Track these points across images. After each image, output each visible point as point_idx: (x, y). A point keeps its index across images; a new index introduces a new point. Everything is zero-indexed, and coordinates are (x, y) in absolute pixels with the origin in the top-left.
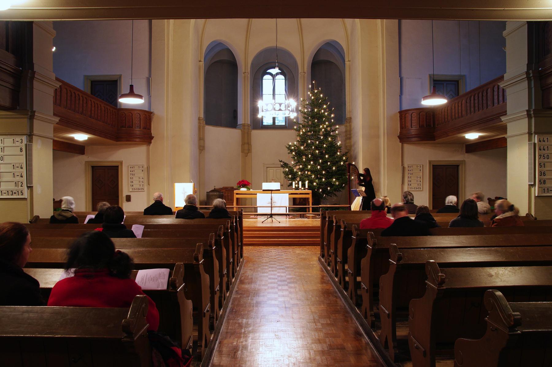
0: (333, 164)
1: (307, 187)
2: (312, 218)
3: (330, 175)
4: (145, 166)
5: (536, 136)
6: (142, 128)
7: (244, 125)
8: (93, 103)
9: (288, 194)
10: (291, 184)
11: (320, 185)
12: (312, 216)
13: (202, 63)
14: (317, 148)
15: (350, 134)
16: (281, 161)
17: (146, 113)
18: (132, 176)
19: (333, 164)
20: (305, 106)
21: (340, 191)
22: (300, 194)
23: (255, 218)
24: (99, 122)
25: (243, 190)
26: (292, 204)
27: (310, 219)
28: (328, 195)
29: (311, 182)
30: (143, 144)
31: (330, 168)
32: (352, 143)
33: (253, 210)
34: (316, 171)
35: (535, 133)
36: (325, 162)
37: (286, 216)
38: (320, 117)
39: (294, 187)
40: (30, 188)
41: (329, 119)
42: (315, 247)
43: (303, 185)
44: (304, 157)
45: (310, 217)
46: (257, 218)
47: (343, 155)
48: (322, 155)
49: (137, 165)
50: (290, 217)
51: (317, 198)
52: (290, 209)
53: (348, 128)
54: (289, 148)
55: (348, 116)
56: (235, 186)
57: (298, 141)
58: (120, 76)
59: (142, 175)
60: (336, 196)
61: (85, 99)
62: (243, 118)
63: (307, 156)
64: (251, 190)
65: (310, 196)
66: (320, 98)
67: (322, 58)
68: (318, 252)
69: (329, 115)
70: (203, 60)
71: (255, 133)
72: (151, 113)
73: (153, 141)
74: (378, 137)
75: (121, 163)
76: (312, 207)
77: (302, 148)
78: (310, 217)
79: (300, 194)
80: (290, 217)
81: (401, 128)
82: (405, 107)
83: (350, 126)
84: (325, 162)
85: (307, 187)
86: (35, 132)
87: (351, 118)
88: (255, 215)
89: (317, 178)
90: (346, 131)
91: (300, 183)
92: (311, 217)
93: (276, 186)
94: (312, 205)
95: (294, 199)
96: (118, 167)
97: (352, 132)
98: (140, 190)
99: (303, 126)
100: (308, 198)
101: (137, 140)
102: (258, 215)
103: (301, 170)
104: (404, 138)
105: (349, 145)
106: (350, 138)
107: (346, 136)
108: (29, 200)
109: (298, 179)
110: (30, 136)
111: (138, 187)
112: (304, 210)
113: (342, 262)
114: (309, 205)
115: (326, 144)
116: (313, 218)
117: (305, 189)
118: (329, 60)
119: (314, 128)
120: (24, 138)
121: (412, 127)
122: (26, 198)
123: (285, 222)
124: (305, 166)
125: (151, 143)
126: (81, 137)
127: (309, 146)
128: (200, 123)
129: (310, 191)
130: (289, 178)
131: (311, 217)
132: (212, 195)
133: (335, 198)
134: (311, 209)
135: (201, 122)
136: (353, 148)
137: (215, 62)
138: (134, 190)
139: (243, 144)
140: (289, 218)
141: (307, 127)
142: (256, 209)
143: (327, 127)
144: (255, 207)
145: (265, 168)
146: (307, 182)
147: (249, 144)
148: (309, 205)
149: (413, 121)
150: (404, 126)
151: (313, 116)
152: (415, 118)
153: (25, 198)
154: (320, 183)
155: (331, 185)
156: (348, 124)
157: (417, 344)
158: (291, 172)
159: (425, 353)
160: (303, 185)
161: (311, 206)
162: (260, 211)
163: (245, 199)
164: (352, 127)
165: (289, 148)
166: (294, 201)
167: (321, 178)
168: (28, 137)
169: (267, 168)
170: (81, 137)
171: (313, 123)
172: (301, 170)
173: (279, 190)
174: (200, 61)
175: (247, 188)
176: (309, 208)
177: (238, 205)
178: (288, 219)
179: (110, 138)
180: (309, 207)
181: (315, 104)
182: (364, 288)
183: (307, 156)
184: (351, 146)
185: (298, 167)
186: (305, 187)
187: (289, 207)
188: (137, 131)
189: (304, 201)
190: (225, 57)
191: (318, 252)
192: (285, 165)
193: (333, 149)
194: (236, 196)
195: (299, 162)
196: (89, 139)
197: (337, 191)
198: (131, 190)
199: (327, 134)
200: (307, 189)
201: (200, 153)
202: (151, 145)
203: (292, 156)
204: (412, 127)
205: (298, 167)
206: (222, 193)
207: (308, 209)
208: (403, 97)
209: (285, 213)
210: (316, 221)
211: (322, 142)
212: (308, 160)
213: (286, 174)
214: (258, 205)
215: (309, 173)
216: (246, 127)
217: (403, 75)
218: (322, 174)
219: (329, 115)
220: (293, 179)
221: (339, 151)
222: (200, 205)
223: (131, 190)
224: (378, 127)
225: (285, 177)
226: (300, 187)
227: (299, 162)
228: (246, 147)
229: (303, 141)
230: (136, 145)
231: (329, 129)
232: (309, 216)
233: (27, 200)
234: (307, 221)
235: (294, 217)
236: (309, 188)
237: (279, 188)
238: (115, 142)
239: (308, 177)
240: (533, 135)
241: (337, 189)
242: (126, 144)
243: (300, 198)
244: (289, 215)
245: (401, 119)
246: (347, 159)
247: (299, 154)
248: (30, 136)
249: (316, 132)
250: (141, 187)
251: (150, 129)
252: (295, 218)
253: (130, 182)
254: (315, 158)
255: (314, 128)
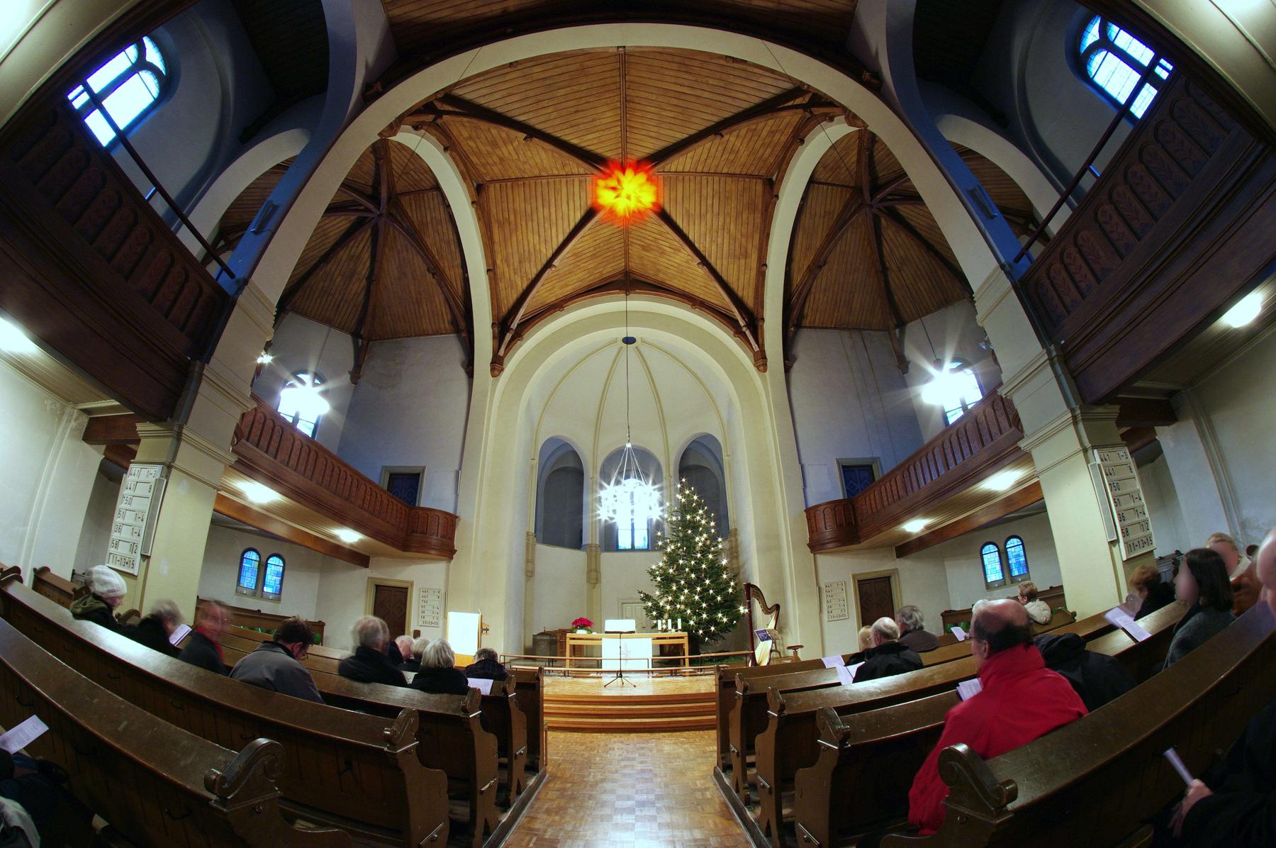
0: (717, 592)
1: (680, 627)
2: (690, 676)
3: (713, 609)
4: (443, 592)
5: (1095, 451)
6: (439, 536)
7: (590, 546)
8: (369, 489)
9: (651, 639)
10: (656, 625)
11: (699, 623)
12: (690, 672)
13: (536, 462)
14: (692, 571)
15: (737, 552)
16: (641, 593)
17: (448, 516)
18: (423, 604)
19: (717, 592)
20: (674, 513)
21: (729, 631)
22: (670, 638)
23: (598, 677)
24: (376, 518)
25: (581, 633)
26: (659, 654)
27: (687, 678)
28: (711, 639)
29: (685, 620)
30: (442, 560)
31: (714, 598)
32: (741, 564)
33: (595, 663)
34: (693, 604)
35: (1094, 447)
36: (705, 590)
37: (648, 673)
38: (695, 526)
39: (660, 628)
40: (145, 557)
41: (707, 530)
42: (701, 732)
43: (675, 626)
44: (674, 584)
45: (686, 674)
46: (601, 677)
47: (730, 580)
48: (700, 581)
49: (432, 589)
50: (655, 675)
51: (695, 644)
52: (654, 661)
53: (733, 544)
54: (652, 573)
55: (732, 526)
56: (570, 627)
57: (665, 562)
58: (424, 469)
59: (436, 603)
60: (724, 639)
61: (355, 481)
62: (591, 536)
63: (678, 583)
64: (594, 633)
65: (685, 641)
66: (693, 501)
67: (692, 462)
68: (708, 749)
69: (708, 523)
70: (537, 458)
71: (606, 557)
72: (457, 517)
73: (454, 556)
74: (778, 548)
75: (412, 584)
76: (689, 658)
77: (671, 571)
78: (686, 674)
79: (670, 638)
80: (655, 675)
81: (811, 531)
82: (812, 503)
83: (736, 540)
84: (705, 590)
85: (680, 627)
86: (177, 463)
87: (736, 530)
88: (598, 672)
89: (694, 613)
90: (731, 548)
91: (670, 621)
92: (688, 674)
93: (629, 625)
94: (689, 655)
95: (662, 646)
96: (407, 588)
97: (739, 548)
98: (433, 625)
99: (671, 542)
100: (682, 645)
101: (433, 552)
102: (602, 672)
103: (671, 603)
104: (816, 546)
105: (737, 566)
106: (737, 557)
107: (732, 554)
108: (141, 579)
109: (666, 616)
110: (168, 467)
111: (431, 619)
112: (677, 663)
113: (773, 791)
114: (684, 655)
115: (706, 577)
116: (692, 674)
117: (676, 631)
118: (700, 464)
119: (688, 543)
120: (158, 468)
121: (826, 529)
122: (136, 574)
123: (646, 686)
124: (676, 597)
125: (452, 559)
126: (349, 536)
127: (680, 569)
128: (528, 539)
129: (686, 634)
130: (652, 615)
131: (688, 674)
132: (541, 640)
133: (720, 642)
134: (687, 661)
135: (531, 538)
136: (742, 571)
137: (557, 470)
138: (426, 624)
139: (589, 571)
140: (653, 677)
141: (678, 541)
142: (599, 664)
143: (706, 539)
144: (598, 660)
145: (620, 604)
146: (679, 621)
147: (597, 571)
148: (684, 655)
149: (827, 521)
150: (815, 529)
151: (686, 525)
152: (830, 516)
153: (133, 575)
154: (700, 620)
155: (716, 623)
156: (733, 539)
157: (807, 834)
158: (656, 606)
159: (770, 792)
160: (675, 626)
161: (687, 656)
162: (605, 666)
163: (592, 646)
164: (739, 542)
165: (652, 573)
166: (663, 650)
167: (700, 615)
168: (165, 468)
169: (623, 603)
170: (349, 536)
171: (686, 536)
172: (671, 603)
173: (633, 632)
174: (534, 459)
175: (588, 630)
176: (684, 659)
177: (575, 656)
178: (651, 679)
179: (393, 545)
180: (684, 659)
181: (685, 509)
182: (764, 787)
183: (678, 583)
184: (739, 568)
185: (665, 599)
186: (677, 627)
187: (652, 659)
188: (434, 540)
189: (677, 649)
190: (571, 464)
191: (708, 749)
192: (647, 598)
193: (715, 570)
194: (569, 643)
195: (667, 592)
196: (361, 541)
197: (725, 632)
198: (421, 623)
199: (705, 551)
200: (680, 630)
201: (527, 581)
202: (453, 561)
203: (656, 583)
204: (826, 529)
205: (665, 599)
206: (554, 638)
207: (682, 661)
208: (808, 490)
209: (647, 669)
210: (697, 680)
211: (699, 562)
212: (680, 589)
213: (649, 610)
214: (603, 657)
215: (683, 607)
216: (594, 548)
217: (803, 462)
218: (701, 608)
219: (708, 523)
220: (660, 616)
221: (725, 572)
222: (525, 654)
223: (421, 623)
224: (778, 536)
225: (646, 614)
226: (670, 627)
227: (667, 591)
228: (593, 574)
229: (672, 559)
230: (432, 560)
231: (708, 542)
232: (685, 672)
233: (136, 579)
234: (682, 682)
235: (661, 675)
236: (684, 629)
237: (634, 629)
238: (400, 552)
239: (682, 612)
240: (1090, 452)
241: (725, 628)
242: (420, 558)
243: (670, 645)
244: (652, 672)
245: (809, 520)
246: (736, 584)
247: (667, 581)
248: (168, 467)
249: (690, 552)
250: (435, 620)
251: (452, 539)
252: (662, 677)
253: (420, 612)
254: (691, 585)
255: (688, 543)
